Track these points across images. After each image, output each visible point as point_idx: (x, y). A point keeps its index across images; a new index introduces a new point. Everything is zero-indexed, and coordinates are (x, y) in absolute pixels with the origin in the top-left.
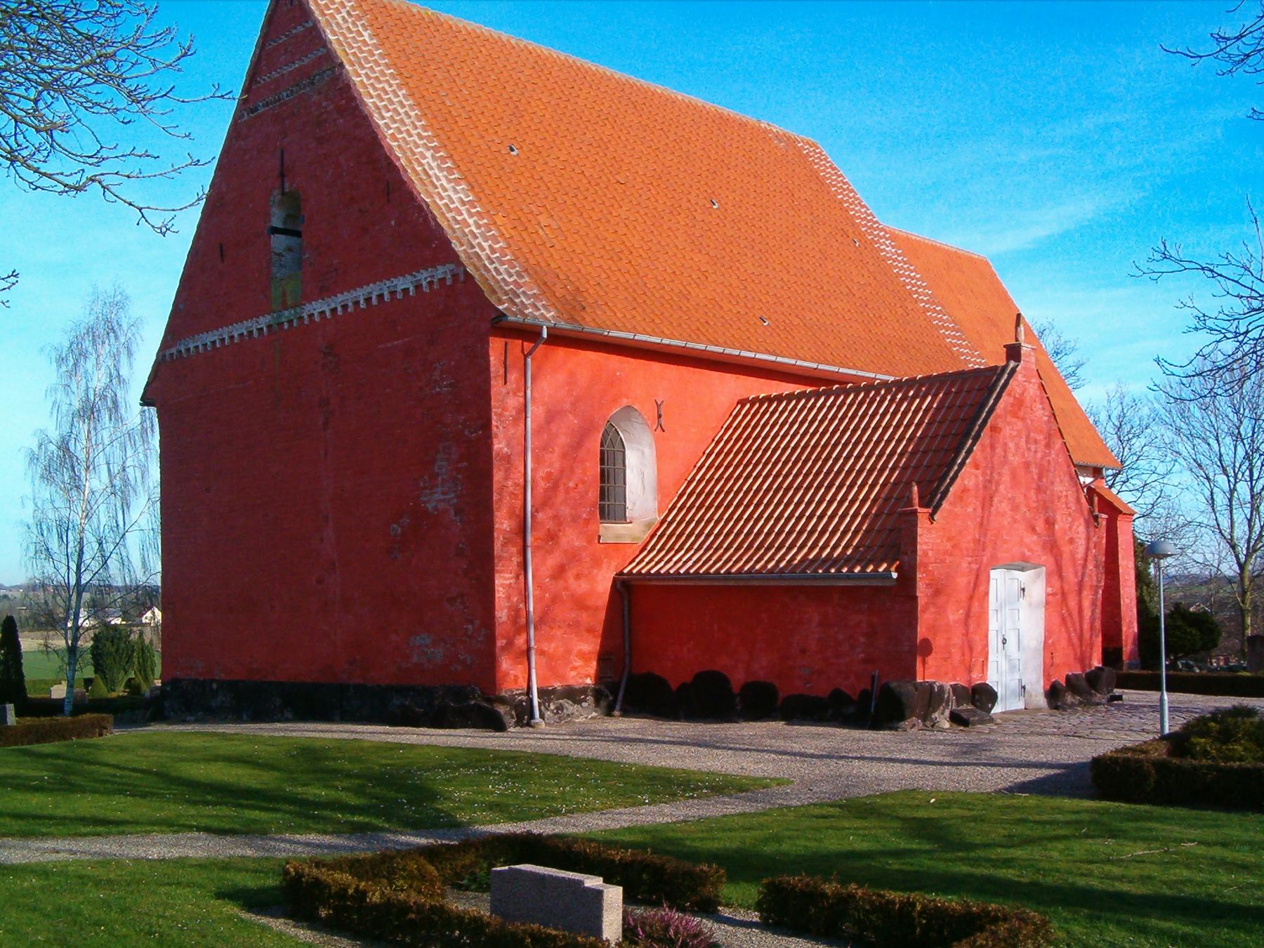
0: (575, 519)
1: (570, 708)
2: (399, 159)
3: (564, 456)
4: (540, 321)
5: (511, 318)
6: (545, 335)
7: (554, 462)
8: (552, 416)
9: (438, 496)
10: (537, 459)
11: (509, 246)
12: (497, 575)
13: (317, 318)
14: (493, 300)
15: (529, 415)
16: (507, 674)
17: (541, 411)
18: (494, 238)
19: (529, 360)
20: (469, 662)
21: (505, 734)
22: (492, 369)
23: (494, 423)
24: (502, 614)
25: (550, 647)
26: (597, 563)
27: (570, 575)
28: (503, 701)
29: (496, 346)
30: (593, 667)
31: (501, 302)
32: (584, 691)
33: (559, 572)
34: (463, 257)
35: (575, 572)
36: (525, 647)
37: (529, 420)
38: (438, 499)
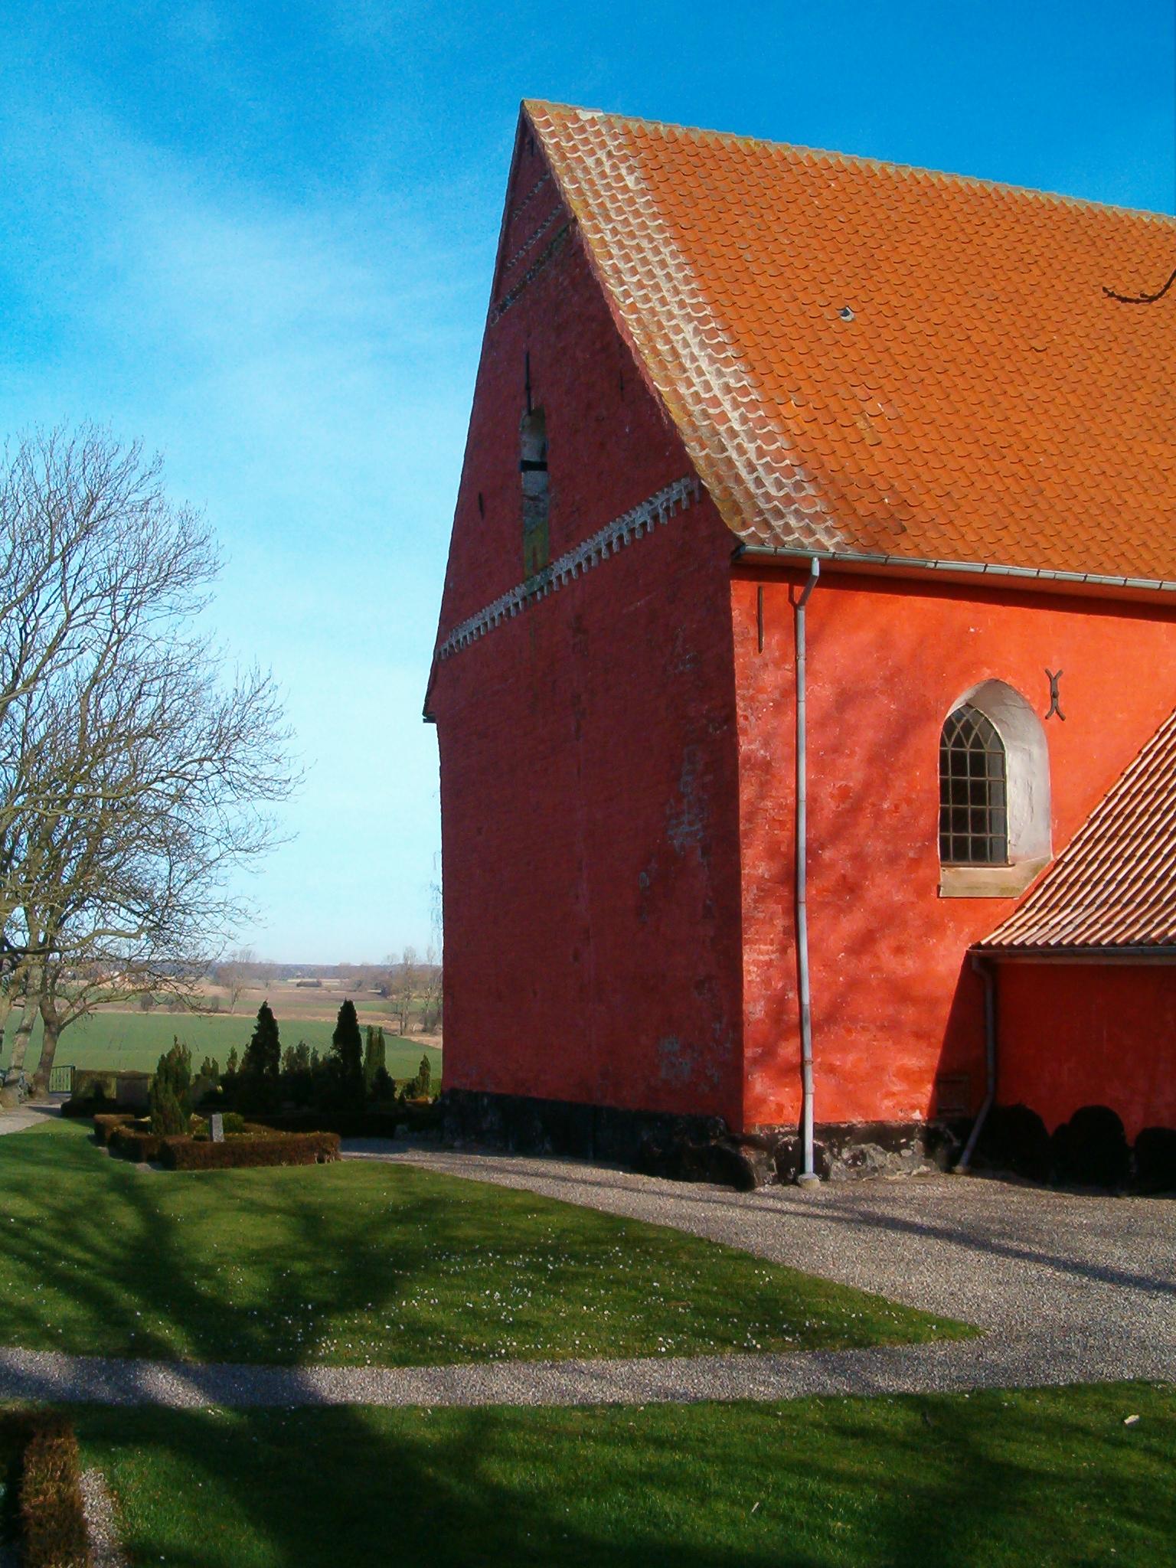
0: (893, 859)
1: (877, 1156)
2: (631, 335)
3: (872, 760)
4: (810, 551)
5: (751, 547)
6: (816, 571)
7: (853, 771)
8: (846, 699)
9: (685, 828)
10: (819, 764)
11: (794, 447)
12: (746, 949)
13: (565, 581)
14: (732, 523)
15: (802, 697)
16: (762, 1101)
17: (826, 691)
18: (770, 438)
19: (802, 613)
20: (716, 1080)
21: (744, 1197)
22: (736, 629)
23: (740, 712)
24: (755, 1009)
25: (848, 1061)
26: (933, 927)
27: (884, 948)
28: (754, 1143)
29: (742, 596)
30: (925, 1093)
31: (745, 525)
32: (908, 1131)
33: (864, 943)
34: (701, 466)
35: (894, 943)
36: (796, 1059)
37: (802, 706)
38: (686, 832)
